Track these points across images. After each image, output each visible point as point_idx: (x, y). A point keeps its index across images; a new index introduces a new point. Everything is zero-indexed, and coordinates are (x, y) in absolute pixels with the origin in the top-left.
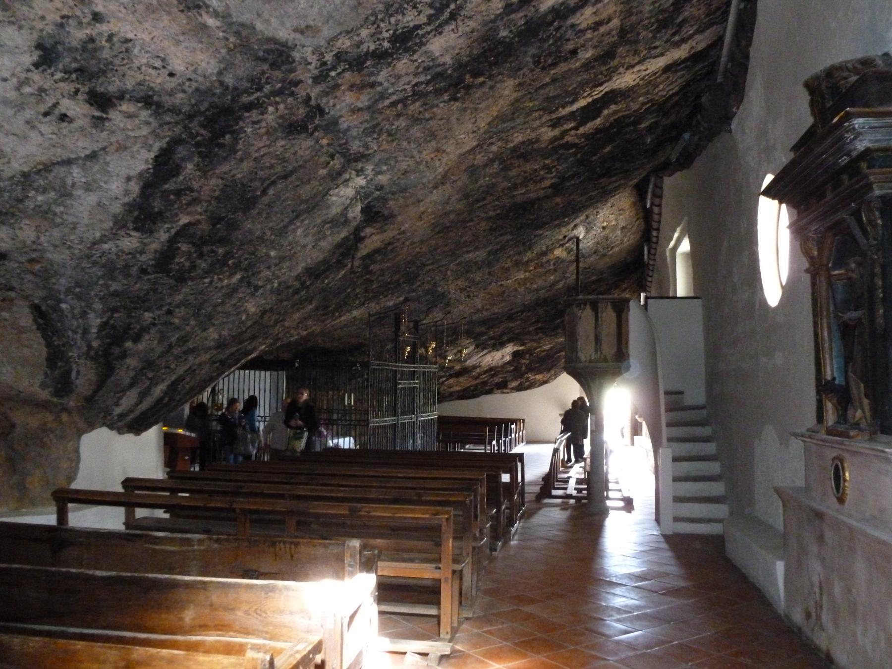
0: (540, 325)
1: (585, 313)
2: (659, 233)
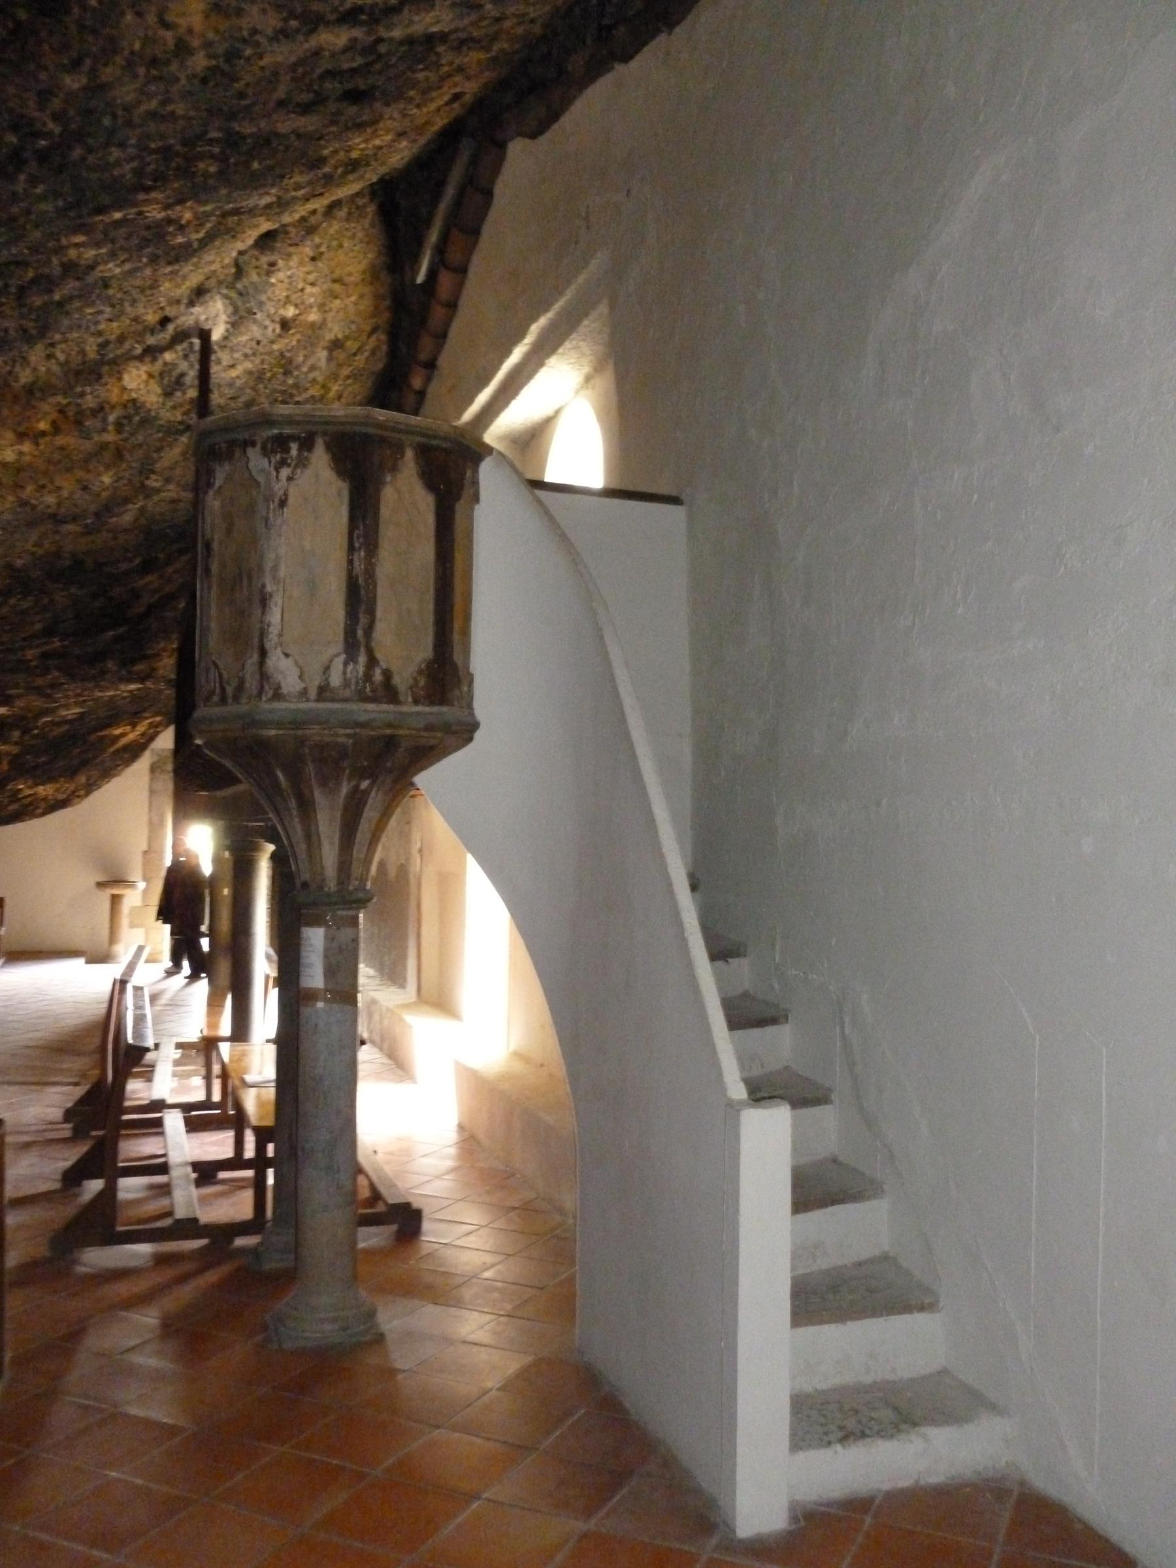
0: (56, 643)
1: (305, 478)
2: (429, 379)
